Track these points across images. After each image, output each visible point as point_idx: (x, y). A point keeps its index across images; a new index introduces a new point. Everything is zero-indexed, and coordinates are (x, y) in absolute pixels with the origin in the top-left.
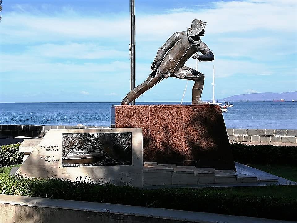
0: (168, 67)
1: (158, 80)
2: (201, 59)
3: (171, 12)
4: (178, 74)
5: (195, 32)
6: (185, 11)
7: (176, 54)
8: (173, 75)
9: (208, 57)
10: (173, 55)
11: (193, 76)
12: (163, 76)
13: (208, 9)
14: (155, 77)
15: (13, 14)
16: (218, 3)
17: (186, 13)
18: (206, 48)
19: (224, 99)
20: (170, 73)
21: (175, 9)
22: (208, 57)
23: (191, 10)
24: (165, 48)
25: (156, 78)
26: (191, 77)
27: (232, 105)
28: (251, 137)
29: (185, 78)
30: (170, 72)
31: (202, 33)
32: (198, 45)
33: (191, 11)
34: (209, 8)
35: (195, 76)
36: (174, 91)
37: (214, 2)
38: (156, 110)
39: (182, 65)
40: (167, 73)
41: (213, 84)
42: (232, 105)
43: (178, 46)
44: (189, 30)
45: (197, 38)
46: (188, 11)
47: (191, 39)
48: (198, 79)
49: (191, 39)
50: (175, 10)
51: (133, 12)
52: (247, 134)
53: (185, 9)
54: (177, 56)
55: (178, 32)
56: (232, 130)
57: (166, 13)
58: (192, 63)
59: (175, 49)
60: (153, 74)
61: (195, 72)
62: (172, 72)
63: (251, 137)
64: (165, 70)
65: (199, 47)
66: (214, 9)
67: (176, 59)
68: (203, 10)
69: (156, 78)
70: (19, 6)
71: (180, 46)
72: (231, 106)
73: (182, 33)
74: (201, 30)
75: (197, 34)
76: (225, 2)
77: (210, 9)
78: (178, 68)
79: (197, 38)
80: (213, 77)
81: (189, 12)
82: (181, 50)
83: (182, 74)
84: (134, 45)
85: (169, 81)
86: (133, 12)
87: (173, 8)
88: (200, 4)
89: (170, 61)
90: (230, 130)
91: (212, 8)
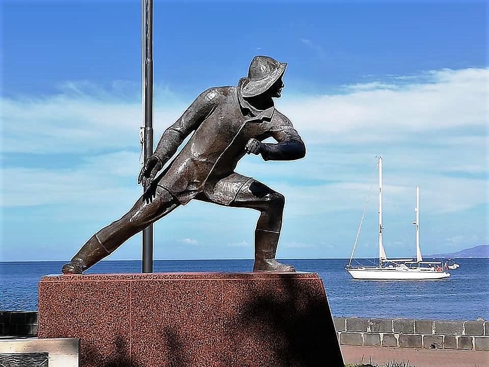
0: (187, 176)
1: (159, 208)
2: (268, 155)
3: (353, 91)
4: (217, 194)
5: (257, 87)
6: (379, 88)
7: (207, 142)
8: (201, 197)
9: (293, 150)
10: (202, 147)
11: (254, 199)
12: (175, 200)
13: (421, 83)
14: (151, 202)
15: (61, 99)
16: (440, 73)
17: (380, 92)
18: (286, 127)
19: (457, 253)
20: (195, 191)
21: (358, 84)
22: (293, 150)
23: (390, 86)
24: (179, 129)
25: (158, 202)
26: (250, 199)
27: (458, 266)
28: (474, 339)
29: (234, 204)
30: (195, 188)
31: (276, 89)
32: (265, 119)
33: (389, 89)
34: (424, 81)
35: (258, 199)
36: (209, 231)
37: (432, 72)
38: (159, 283)
39: (226, 168)
40: (187, 192)
41: (418, 224)
42: (458, 266)
43: (213, 122)
44: (243, 82)
45: (264, 100)
46: (383, 89)
47: (245, 104)
48: (268, 204)
49: (245, 104)
50: (360, 86)
51: (149, 53)
52: (463, 333)
53: (378, 85)
54: (212, 147)
55: (214, 89)
56: (430, 324)
57: (343, 93)
58: (251, 166)
59: (206, 130)
60: (148, 195)
61: (259, 189)
62: (200, 189)
63: (474, 339)
64: (179, 182)
65: (268, 125)
66: (434, 83)
67: (210, 154)
68: (412, 86)
69: (158, 202)
70: (71, 85)
71: (219, 123)
72: (456, 266)
73: (225, 91)
74: (272, 80)
75: (261, 91)
76: (454, 71)
77: (425, 83)
78: (214, 179)
79: (264, 100)
80: (417, 210)
81: (387, 91)
82: (220, 132)
83: (225, 193)
84: (152, 131)
85: (193, 208)
86: (149, 53)
87: (355, 83)
88: (406, 75)
89: (192, 160)
90: (428, 323)
91: (429, 83)
